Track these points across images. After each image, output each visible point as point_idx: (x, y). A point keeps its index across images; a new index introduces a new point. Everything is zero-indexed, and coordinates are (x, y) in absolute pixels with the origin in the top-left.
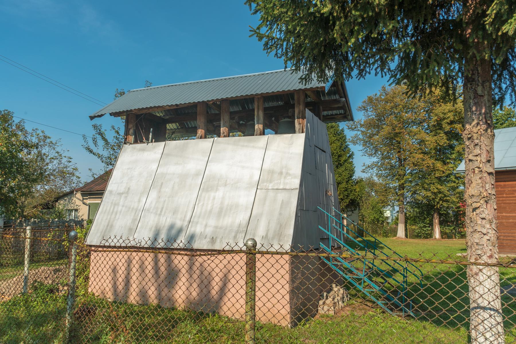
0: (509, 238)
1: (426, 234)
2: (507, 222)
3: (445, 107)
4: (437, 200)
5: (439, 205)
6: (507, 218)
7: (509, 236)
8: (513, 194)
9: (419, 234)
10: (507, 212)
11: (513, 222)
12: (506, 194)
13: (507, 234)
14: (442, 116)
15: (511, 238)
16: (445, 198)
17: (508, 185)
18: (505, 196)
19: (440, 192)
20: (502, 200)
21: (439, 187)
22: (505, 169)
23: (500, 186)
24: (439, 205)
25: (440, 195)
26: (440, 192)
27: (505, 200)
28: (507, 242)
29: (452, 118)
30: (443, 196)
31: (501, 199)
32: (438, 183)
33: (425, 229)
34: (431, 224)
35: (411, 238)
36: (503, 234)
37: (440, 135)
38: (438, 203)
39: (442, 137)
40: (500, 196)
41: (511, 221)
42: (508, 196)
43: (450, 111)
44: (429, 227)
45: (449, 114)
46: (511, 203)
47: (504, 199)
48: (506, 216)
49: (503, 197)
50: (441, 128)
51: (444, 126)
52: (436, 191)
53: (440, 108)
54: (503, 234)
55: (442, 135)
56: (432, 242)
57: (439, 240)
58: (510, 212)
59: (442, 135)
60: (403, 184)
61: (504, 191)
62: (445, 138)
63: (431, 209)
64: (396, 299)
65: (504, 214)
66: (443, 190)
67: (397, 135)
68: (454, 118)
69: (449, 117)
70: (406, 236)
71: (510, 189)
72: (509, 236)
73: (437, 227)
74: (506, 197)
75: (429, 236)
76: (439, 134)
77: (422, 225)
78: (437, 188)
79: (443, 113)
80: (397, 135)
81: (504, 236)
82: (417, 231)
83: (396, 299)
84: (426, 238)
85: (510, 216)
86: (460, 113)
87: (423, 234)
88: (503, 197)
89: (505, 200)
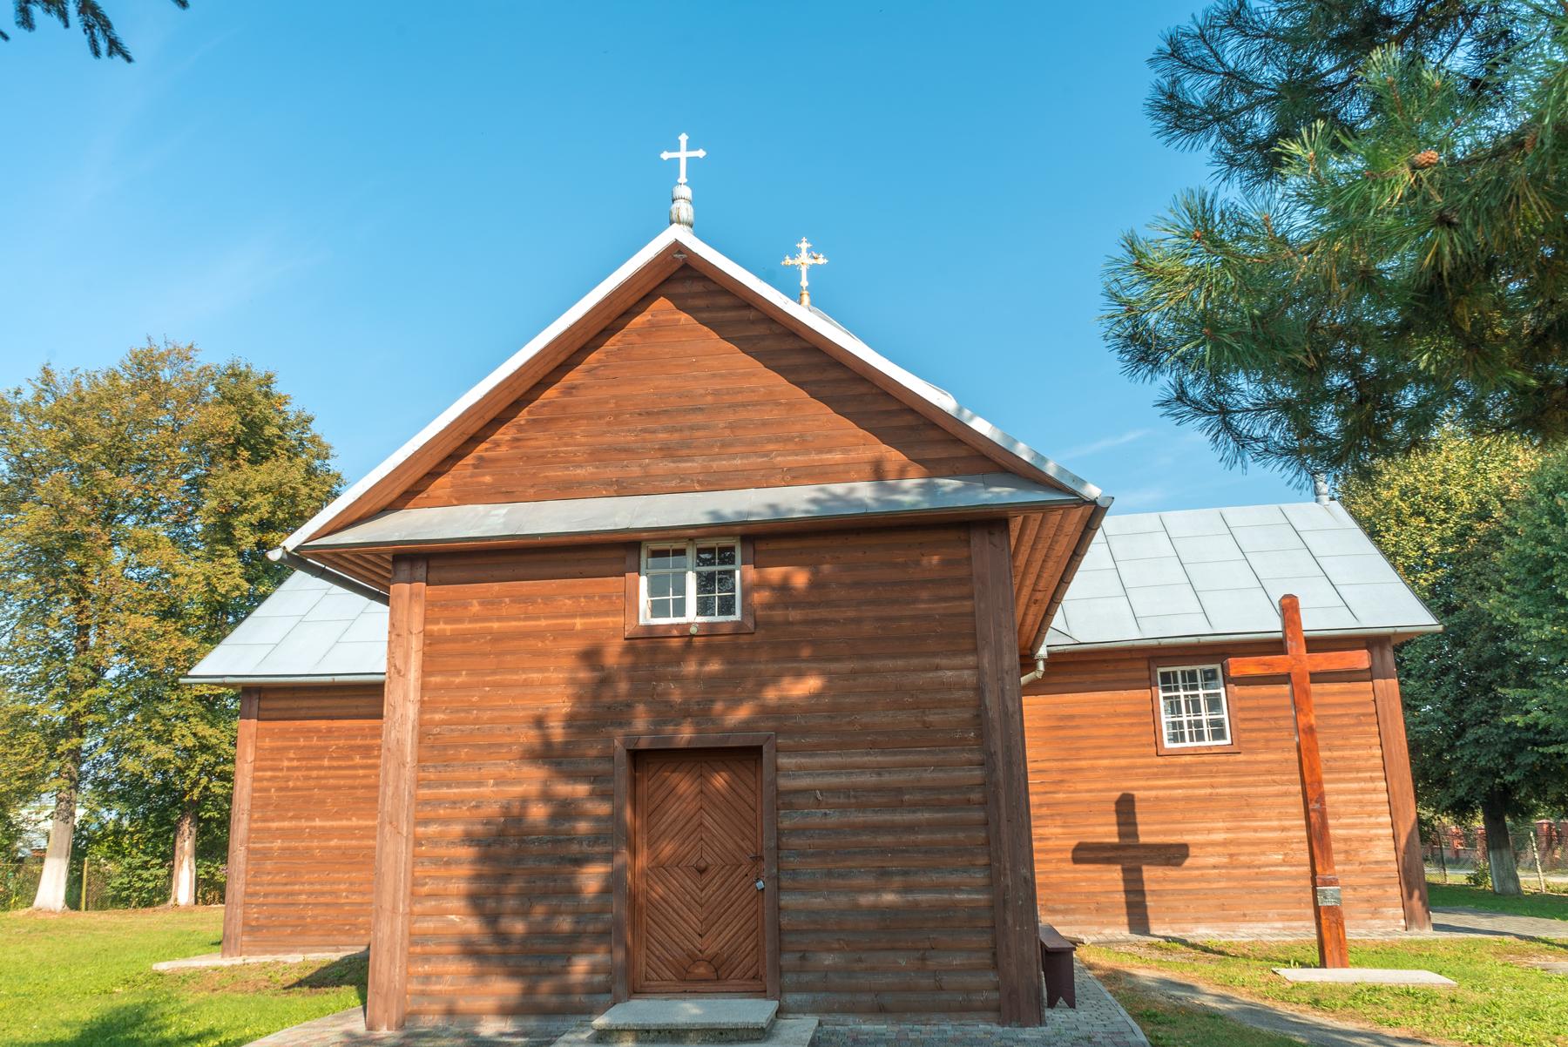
0: (322, 900)
1: (149, 892)
2: (322, 848)
3: (253, 473)
4: (192, 774)
5: (196, 792)
6: (326, 833)
7: (323, 893)
8: (349, 758)
9: (124, 894)
10: (326, 816)
11: (338, 848)
12: (331, 758)
13: (318, 887)
14: (234, 499)
15: (328, 899)
16: (218, 769)
17: (339, 729)
18: (326, 763)
19: (204, 748)
20: (318, 778)
21: (203, 729)
22: (329, 679)
23: (318, 731)
24: (196, 792)
25: (201, 759)
26: (204, 748)
27: (325, 778)
28: (316, 912)
29: (264, 512)
30: (213, 759)
31: (314, 774)
32: (203, 718)
33: (145, 875)
34: (168, 858)
35: (101, 904)
36: (307, 887)
37: (224, 560)
38: (195, 784)
39: (229, 566)
40: (314, 763)
41: (333, 843)
42: (335, 764)
43: (264, 490)
44: (162, 867)
45: (259, 499)
46: (339, 788)
47: (322, 773)
48: (322, 828)
49: (321, 768)
50: (229, 540)
51: (237, 534)
52: (190, 742)
53: (232, 475)
54: (307, 887)
55: (229, 561)
56: (168, 916)
57: (187, 909)
58: (338, 815)
59: (229, 561)
60: (77, 714)
61: (326, 748)
62: (237, 571)
63: (173, 804)
64: (1205, 716)
65: (318, 823)
66: (214, 741)
67: (74, 541)
68: (274, 513)
69: (256, 508)
70: (73, 902)
71: (342, 742)
72: (323, 893)
73: (185, 864)
74: (330, 768)
75: (159, 895)
76: (221, 556)
77: (137, 862)
78: (195, 735)
79: (239, 492)
80: (74, 541)
81: (310, 894)
82: (116, 883)
83: (1205, 716)
84: (148, 904)
85: (332, 828)
86: (293, 498)
87: (141, 889)
88: (321, 768)
89: (325, 778)
